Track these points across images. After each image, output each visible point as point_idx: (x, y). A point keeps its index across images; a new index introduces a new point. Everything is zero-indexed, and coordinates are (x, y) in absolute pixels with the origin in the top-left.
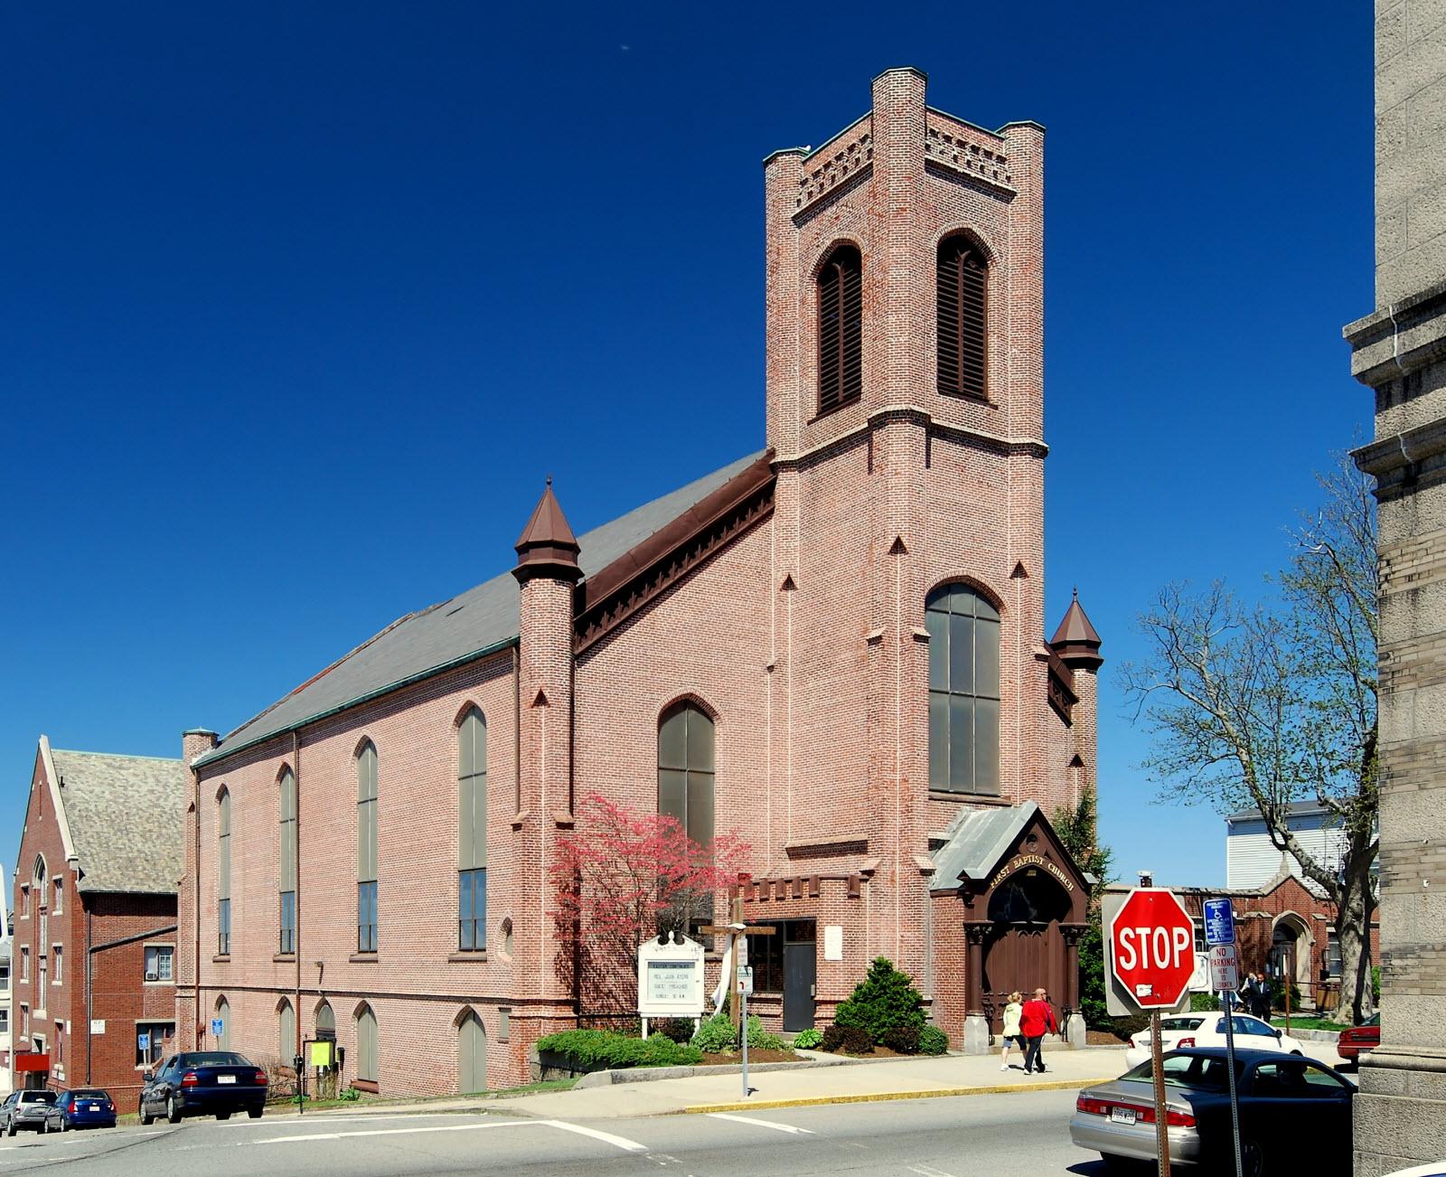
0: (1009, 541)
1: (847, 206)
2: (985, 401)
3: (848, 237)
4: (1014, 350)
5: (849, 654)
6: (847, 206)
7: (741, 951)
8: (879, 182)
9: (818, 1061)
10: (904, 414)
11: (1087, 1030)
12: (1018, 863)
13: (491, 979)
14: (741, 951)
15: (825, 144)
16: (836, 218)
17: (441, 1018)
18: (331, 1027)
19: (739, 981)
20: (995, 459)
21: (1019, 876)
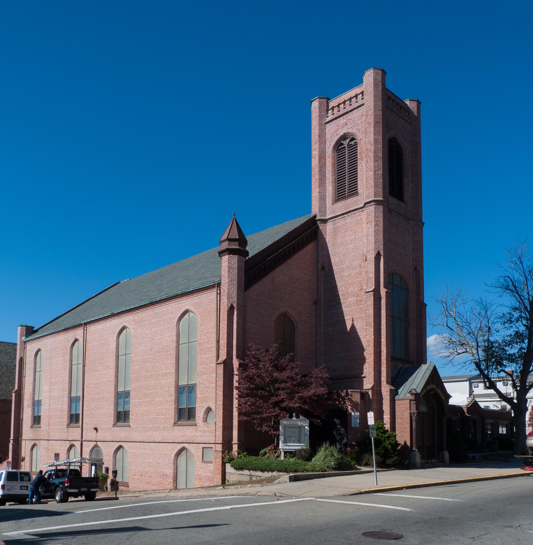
0: (412, 259)
1: (351, 120)
2: (403, 201)
3: (352, 132)
4: (412, 184)
5: (353, 299)
6: (351, 120)
7: (370, 418)
8: (369, 110)
9: (362, 470)
10: (381, 202)
11: (102, 459)
12: (428, 388)
13: (199, 434)
14: (370, 418)
15: (335, 98)
16: (345, 124)
17: (168, 453)
18: (101, 458)
19: (370, 432)
20: (117, 331)
21: (428, 391)
